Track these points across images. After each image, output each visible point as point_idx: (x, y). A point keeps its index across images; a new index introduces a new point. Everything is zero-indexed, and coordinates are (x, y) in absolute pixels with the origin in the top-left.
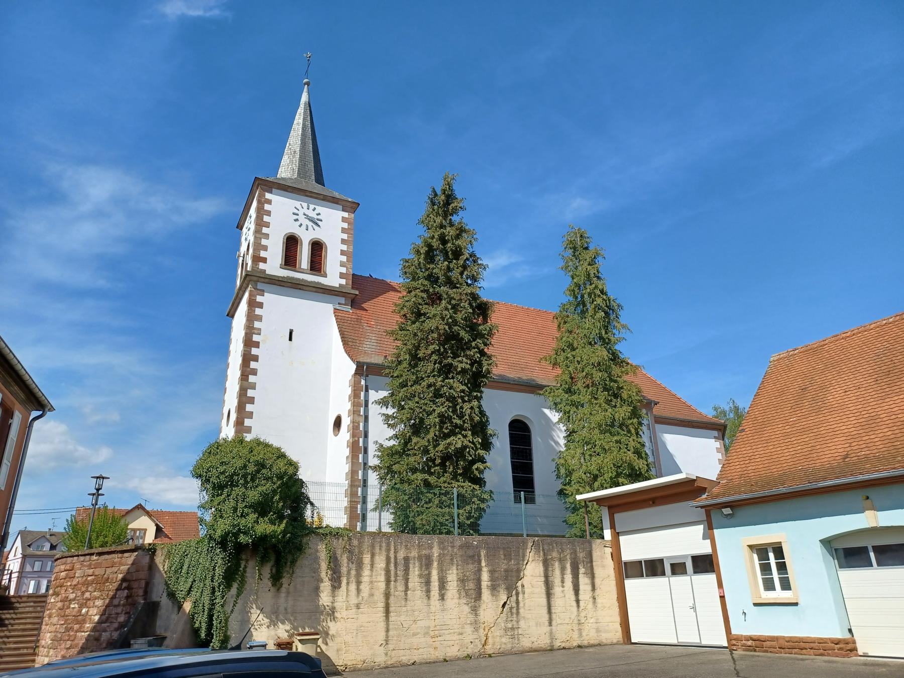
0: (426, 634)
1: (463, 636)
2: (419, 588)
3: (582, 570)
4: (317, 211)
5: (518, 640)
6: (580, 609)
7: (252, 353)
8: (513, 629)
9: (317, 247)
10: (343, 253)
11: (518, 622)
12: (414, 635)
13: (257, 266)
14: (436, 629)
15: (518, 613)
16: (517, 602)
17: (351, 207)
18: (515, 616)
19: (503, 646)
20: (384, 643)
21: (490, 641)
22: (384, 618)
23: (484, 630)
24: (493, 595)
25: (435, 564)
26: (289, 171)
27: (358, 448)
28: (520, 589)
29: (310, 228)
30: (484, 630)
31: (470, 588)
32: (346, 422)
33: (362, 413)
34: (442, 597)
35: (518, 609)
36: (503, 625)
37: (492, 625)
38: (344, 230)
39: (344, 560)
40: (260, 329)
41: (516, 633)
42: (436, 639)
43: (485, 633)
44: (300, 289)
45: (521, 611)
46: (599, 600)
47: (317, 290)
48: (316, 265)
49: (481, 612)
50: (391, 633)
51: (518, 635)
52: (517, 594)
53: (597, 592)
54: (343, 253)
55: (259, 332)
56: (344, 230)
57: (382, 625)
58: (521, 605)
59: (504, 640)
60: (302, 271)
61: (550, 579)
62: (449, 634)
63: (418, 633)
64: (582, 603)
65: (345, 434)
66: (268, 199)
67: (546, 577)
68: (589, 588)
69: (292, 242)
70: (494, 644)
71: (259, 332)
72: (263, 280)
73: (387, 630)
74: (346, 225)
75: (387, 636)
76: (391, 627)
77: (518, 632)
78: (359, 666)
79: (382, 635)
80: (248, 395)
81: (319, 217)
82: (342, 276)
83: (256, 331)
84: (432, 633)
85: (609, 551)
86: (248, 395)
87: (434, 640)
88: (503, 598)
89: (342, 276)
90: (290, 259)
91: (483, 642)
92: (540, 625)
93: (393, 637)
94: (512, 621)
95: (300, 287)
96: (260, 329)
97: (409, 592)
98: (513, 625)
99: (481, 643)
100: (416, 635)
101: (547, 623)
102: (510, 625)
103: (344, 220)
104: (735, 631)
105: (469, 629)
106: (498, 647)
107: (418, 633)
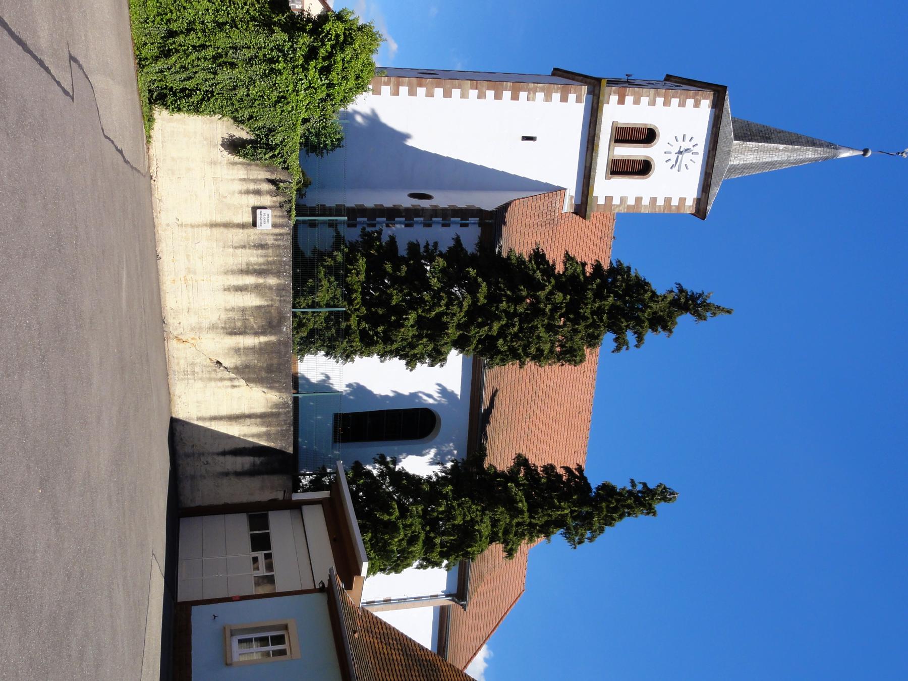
0: (189, 270)
1: (186, 313)
2: (236, 262)
3: (258, 460)
4: (690, 164)
5: (182, 379)
6: (215, 457)
7: (504, 92)
8: (194, 373)
9: (644, 168)
10: (639, 200)
11: (201, 379)
12: (188, 256)
13: (612, 93)
14: (194, 281)
15: (210, 379)
16: (222, 379)
17: (700, 211)
18: (208, 376)
19: (176, 361)
20: (179, 223)
21: (181, 346)
22: (205, 222)
23: (193, 339)
24: (230, 349)
25: (260, 281)
26: (742, 132)
27: (392, 214)
28: (236, 383)
29: (668, 156)
30: (193, 339)
31: (236, 323)
32: (424, 204)
33: (434, 219)
34: (228, 289)
35: (215, 380)
36: (198, 361)
37: (198, 348)
38: (668, 200)
39: (264, 252)
40: (534, 100)
41: (189, 377)
42: (183, 282)
43: (190, 339)
44: (587, 148)
45: (213, 384)
46: (225, 481)
47: (588, 169)
48: (619, 169)
49: (211, 335)
50: (189, 230)
51: (188, 379)
52: (231, 379)
53: (234, 480)
54: (639, 200)
55: (531, 99)
56: (668, 200)
57: (198, 220)
58: (219, 384)
59: (182, 362)
60: (611, 149)
61: (248, 420)
62: (188, 296)
63: (189, 261)
64: (221, 459)
65: (408, 203)
66: (700, 104)
67: (250, 416)
68: (239, 468)
69: (648, 136)
70: (178, 350)
71: (531, 99)
72: (595, 101)
73: (192, 226)
74: (675, 203)
75: (186, 225)
76: (196, 230)
77: (190, 379)
78: (156, 195)
79: (187, 219)
80: (453, 90)
81: (683, 166)
82: (609, 199)
83: (531, 95)
84: (189, 277)
85: (280, 496)
86: (453, 90)
87: (183, 279)
88: (227, 362)
89: (609, 199)
90: (624, 135)
91: (180, 337)
92: (198, 406)
93: (185, 232)
94: (202, 372)
95: (590, 146)
96: (534, 100)
97: (231, 250)
98: (197, 373)
99: (179, 335)
100: (187, 258)
101: (200, 415)
102: (197, 369)
103: (682, 200)
104: (194, 609)
105: (193, 320)
106: (175, 355)
107: (189, 261)
